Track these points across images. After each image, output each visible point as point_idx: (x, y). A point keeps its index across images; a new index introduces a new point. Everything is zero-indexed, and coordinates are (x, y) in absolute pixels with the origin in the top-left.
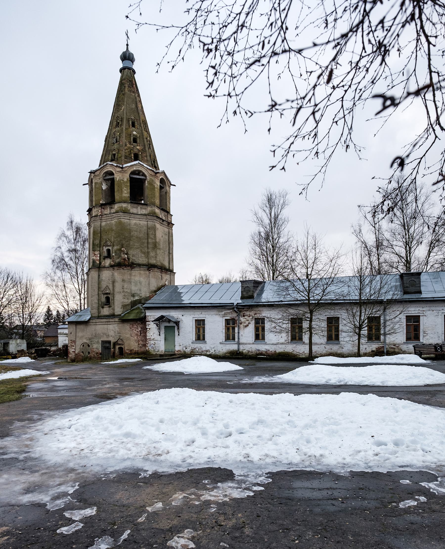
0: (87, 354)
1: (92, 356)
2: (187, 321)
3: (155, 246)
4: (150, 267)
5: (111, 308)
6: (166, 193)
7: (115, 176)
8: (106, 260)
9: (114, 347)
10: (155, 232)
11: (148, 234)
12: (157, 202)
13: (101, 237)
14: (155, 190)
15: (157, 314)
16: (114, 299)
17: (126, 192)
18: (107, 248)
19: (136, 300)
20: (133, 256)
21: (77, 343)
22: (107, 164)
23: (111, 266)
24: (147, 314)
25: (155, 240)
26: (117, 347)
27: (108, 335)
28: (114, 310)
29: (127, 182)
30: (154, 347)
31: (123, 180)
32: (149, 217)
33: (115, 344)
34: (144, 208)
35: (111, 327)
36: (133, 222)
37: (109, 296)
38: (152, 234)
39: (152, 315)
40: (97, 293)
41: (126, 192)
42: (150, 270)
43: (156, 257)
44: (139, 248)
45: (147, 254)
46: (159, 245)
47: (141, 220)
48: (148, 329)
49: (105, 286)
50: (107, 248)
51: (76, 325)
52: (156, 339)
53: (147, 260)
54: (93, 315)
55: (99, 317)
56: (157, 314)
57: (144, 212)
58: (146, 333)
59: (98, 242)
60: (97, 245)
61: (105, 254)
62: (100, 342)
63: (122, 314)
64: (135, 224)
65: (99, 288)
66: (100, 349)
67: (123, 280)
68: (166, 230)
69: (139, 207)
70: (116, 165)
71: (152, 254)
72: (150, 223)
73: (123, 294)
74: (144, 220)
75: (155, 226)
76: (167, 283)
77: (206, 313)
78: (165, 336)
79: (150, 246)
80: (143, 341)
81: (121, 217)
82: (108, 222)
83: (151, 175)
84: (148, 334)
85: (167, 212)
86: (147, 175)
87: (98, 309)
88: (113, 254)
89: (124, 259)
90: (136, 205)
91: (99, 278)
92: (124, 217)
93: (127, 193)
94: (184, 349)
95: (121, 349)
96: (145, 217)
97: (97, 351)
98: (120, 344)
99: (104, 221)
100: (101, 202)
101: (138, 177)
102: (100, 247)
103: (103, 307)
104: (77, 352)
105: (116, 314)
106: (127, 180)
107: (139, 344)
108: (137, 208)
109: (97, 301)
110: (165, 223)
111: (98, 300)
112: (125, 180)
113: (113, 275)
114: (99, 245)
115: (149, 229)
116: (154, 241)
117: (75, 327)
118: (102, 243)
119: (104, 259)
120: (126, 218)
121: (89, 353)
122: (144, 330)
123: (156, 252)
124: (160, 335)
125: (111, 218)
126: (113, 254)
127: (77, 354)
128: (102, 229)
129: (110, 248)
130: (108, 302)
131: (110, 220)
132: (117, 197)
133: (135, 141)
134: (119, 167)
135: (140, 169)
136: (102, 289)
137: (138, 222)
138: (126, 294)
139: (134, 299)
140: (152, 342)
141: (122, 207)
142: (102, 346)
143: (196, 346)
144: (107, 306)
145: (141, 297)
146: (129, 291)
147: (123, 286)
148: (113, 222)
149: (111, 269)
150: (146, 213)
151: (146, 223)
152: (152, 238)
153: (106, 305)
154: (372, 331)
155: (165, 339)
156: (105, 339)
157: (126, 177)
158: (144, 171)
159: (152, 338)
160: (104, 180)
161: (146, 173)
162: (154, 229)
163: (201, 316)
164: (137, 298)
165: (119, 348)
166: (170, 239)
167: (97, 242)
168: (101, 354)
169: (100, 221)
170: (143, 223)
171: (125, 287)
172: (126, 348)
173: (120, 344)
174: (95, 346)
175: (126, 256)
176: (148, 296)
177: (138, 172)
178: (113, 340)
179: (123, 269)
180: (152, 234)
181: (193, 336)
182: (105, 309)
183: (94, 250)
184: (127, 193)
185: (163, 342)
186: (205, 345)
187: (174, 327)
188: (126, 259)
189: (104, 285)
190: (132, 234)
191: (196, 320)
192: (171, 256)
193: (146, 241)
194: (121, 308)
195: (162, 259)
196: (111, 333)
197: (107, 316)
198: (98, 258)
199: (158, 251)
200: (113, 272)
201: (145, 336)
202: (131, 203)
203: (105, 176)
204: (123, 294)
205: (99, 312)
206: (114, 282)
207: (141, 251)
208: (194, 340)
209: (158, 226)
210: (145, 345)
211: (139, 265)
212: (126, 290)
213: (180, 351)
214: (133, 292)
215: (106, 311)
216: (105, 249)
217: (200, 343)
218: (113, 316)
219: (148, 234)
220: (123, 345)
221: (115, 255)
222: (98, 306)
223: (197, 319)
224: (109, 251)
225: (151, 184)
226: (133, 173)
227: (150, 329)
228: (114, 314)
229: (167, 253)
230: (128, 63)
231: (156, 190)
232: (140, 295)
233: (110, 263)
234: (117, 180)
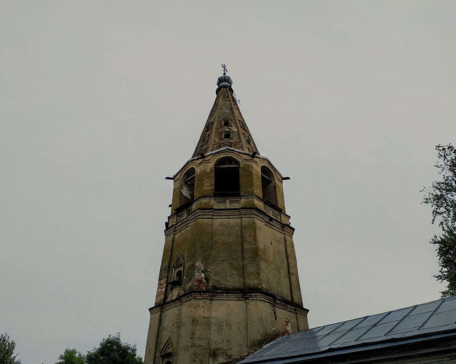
3: (256, 254)
4: (245, 292)
6: (275, 187)
10: (255, 232)
11: (242, 237)
12: (258, 191)
14: (252, 177)
17: (208, 184)
18: (178, 270)
20: (217, 274)
23: (179, 298)
25: (256, 245)
29: (210, 173)
32: (242, 211)
36: (218, 221)
38: (250, 236)
42: (247, 299)
43: (259, 274)
45: (242, 271)
46: (265, 253)
47: (230, 217)
53: (241, 279)
57: (236, 206)
64: (221, 224)
68: (280, 236)
71: (251, 269)
72: (246, 220)
73: (192, 350)
74: (237, 217)
75: (254, 223)
76: (289, 328)
79: (247, 255)
81: (199, 217)
85: (281, 211)
86: (240, 161)
89: (200, 281)
92: (203, 217)
93: (210, 185)
96: (236, 212)
102: (168, 271)
106: (211, 169)
110: (274, 223)
112: (209, 170)
114: (167, 269)
115: (245, 228)
116: (253, 246)
120: (207, 217)
123: (258, 265)
128: (175, 243)
129: (181, 269)
135: (229, 155)
137: (226, 221)
138: (199, 352)
145: (230, 357)
146: (204, 343)
147: (193, 334)
151: (238, 220)
152: (250, 243)
157: (210, 166)
158: (235, 157)
160: (186, 183)
161: (238, 159)
162: (253, 227)
166: (289, 250)
170: (234, 221)
171: (197, 334)
175: (203, 275)
177: (230, 160)
179: (195, 298)
180: (250, 236)
184: (210, 185)
190: (215, 239)
192: (293, 279)
193: (239, 248)
195: (269, 277)
198: (164, 290)
199: (263, 265)
204: (192, 350)
207: (232, 266)
209: (259, 223)
211: (227, 291)
212: (198, 343)
214: (213, 347)
219: (242, 237)
224: (179, 273)
225: (249, 171)
226: (221, 162)
229: (284, 272)
230: (223, 222)
231: (254, 177)
232: (229, 353)
233: (179, 293)
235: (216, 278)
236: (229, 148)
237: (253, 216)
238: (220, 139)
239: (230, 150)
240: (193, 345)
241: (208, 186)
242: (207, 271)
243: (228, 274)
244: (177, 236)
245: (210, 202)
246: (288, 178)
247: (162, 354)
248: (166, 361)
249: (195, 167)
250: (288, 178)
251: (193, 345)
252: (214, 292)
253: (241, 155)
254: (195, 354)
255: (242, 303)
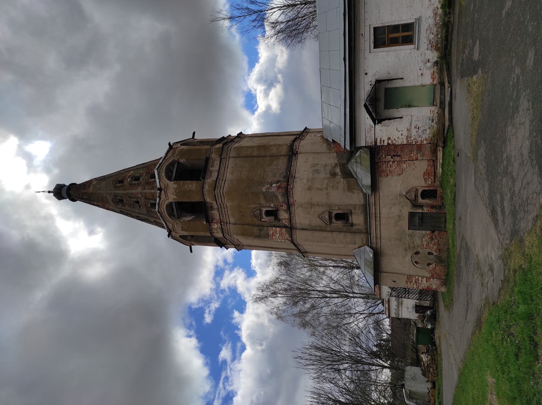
0: (431, 257)
1: (435, 247)
2: (378, 63)
5: (353, 211)
7: (171, 200)
8: (281, 217)
9: (421, 206)
11: (246, 157)
13: (249, 225)
15: (364, 119)
16: (338, 206)
17: (190, 185)
18: (264, 215)
19: (342, 171)
21: (412, 273)
22: (158, 211)
24: (363, 144)
25: (255, 147)
26: (420, 200)
27: (399, 216)
28: (355, 206)
30: (422, 129)
31: (176, 189)
32: (223, 156)
33: (415, 205)
34: (213, 163)
35: (384, 211)
37: (333, 214)
39: (370, 132)
40: (329, 234)
41: (190, 185)
42: (297, 152)
43: (278, 145)
44: (264, 168)
47: (226, 167)
48: (390, 142)
49: (319, 220)
50: (264, 215)
51: (381, 272)
52: (408, 125)
53: (282, 158)
54: (365, 242)
55: (368, 232)
56: (364, 119)
57: (217, 163)
58: (395, 146)
59: (256, 228)
60: (260, 230)
61: (272, 218)
62: (411, 231)
63: (362, 191)
65: (321, 230)
66: (424, 232)
67: (309, 189)
69: (211, 169)
70: (158, 199)
71: (274, 151)
74: (227, 162)
77: (362, 25)
78: (402, 107)
80: (411, 152)
81: (221, 192)
82: (229, 212)
83: (172, 155)
84: (400, 142)
86: (173, 159)
87: (355, 233)
88: (272, 205)
89: (279, 187)
90: (208, 173)
91: (307, 230)
94: (429, 65)
95: (426, 194)
96: (224, 161)
97: (427, 238)
98: (416, 196)
99: (228, 219)
100: (205, 223)
101: (174, 172)
102: (263, 226)
103: (352, 225)
104: (428, 275)
105: (362, 202)
107: (417, 159)
108: (211, 172)
109: (342, 234)
111: (340, 232)
112: (175, 186)
113: (301, 206)
116: (255, 149)
117: (384, 274)
118: (258, 222)
119: (279, 220)
120: (223, 185)
121: (430, 253)
122: (394, 150)
123: (271, 146)
124: (401, 118)
125: (226, 211)
126: (272, 205)
127: (432, 275)
128: (238, 222)
130: (343, 217)
131: (226, 209)
132: (196, 199)
133: (137, 179)
134: (160, 194)
135: (165, 168)
136: (323, 224)
137: (229, 170)
139: (340, 174)
140: (414, 132)
141: (208, 191)
142: (419, 230)
143: (425, 40)
144: (350, 218)
147: (318, 189)
148: (228, 205)
149: (292, 209)
150: (219, 159)
151: (231, 160)
153: (348, 220)
154: (397, 38)
155: (410, 106)
156: (405, 223)
157: (172, 185)
159: (405, 133)
160: (178, 218)
163: (367, 35)
164: (338, 170)
165: (423, 197)
167: (256, 230)
168: (433, 232)
169: (228, 225)
170: (231, 163)
172: (423, 183)
173: (416, 196)
174: (418, 241)
175: (274, 185)
176: (335, 154)
178: (407, 209)
181: (405, 50)
182: (354, 222)
183: (267, 236)
185: (413, 111)
186: (423, 19)
187: (386, 89)
188: (278, 185)
189: (318, 222)
191: (374, 48)
194: (353, 192)
196: (395, 211)
197: (366, 219)
198: (278, 229)
200: (296, 206)
201: (402, 146)
202: (204, 178)
203: (174, 216)
205: (359, 232)
206: (312, 205)
208: (412, 46)
210: (420, 147)
213: (433, 74)
215: (357, 219)
216: (265, 219)
217: (419, 31)
218: (366, 208)
219: (246, 157)
220: (417, 190)
221: (272, 202)
222: (350, 232)
223: (372, 45)
224: (268, 213)
227: (389, 139)
228: (362, 205)
233: (284, 210)
234: (175, 197)
235: (278, 176)
236: (157, 167)
237: (229, 148)
238: (139, 185)
239: (159, 167)
240: (327, 189)
241: (192, 186)
242: (272, 182)
243: (276, 167)
244: (232, 220)
245: (274, 24)
246: (194, 133)
247: (328, 224)
248: (334, 220)
249: (167, 202)
250: (194, 133)
251: (327, 189)
252: (288, 177)
253: (167, 158)
254: (332, 187)
255: (300, 156)
